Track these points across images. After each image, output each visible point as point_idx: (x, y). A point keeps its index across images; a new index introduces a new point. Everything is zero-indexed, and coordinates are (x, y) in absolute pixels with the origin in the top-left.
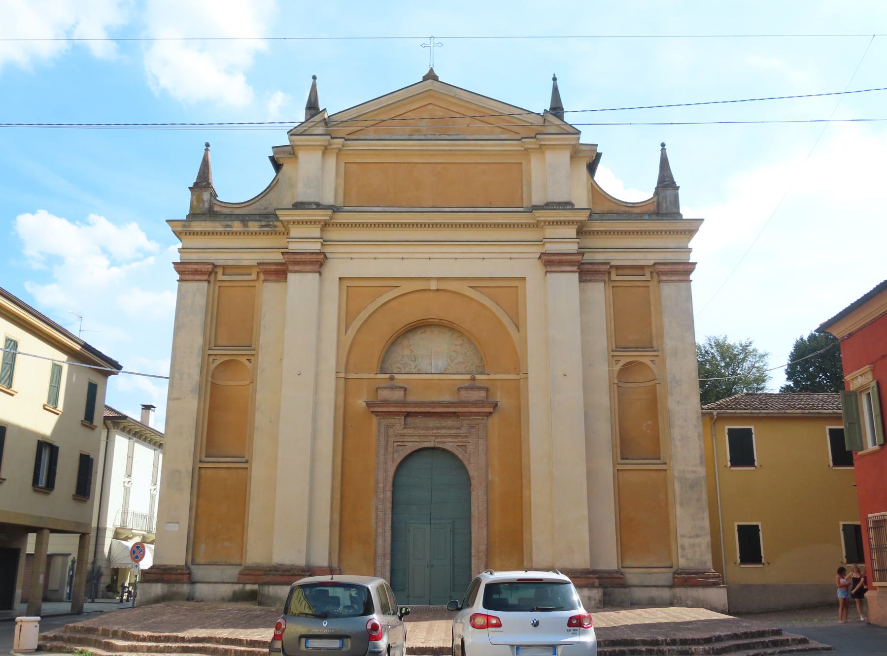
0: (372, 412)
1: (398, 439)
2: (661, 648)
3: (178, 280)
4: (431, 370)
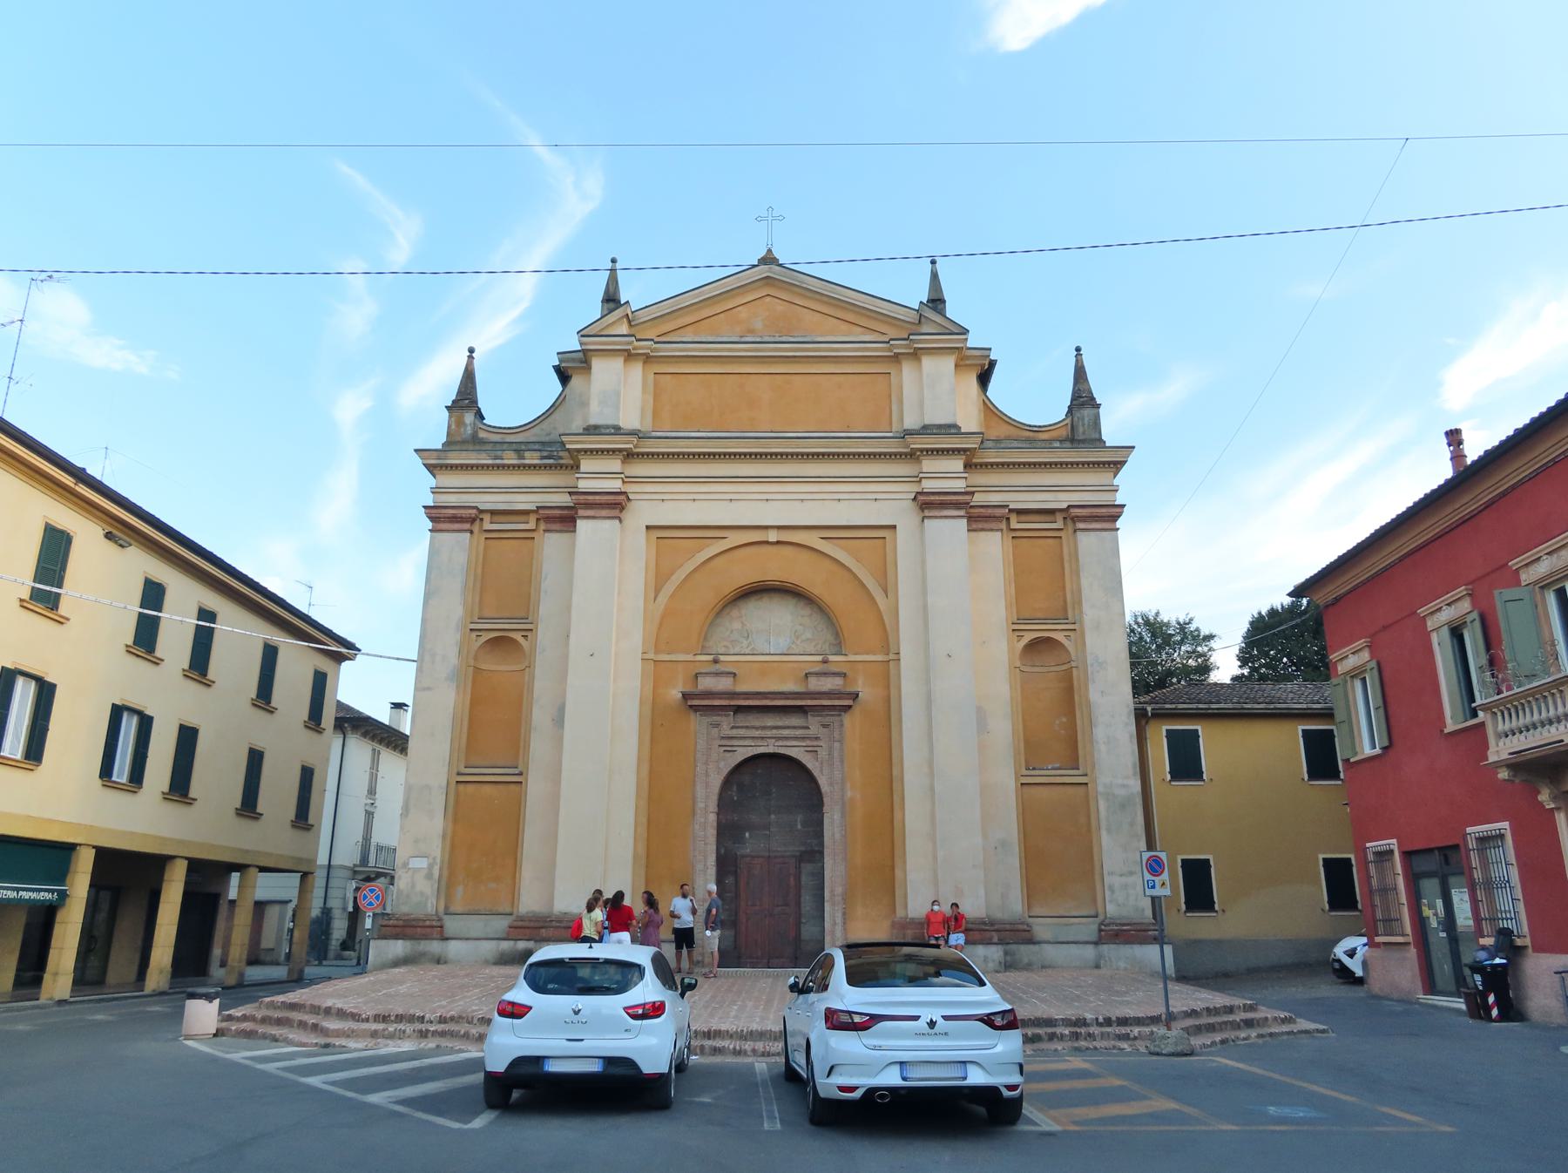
0: (691, 706)
2: (1091, 1030)
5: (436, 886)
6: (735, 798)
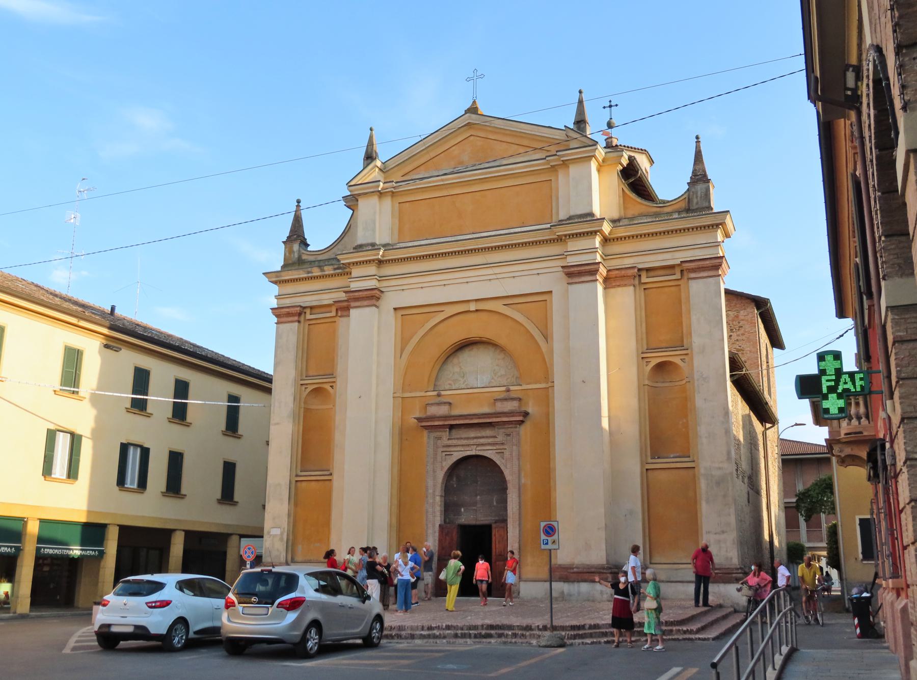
1: (445, 449)
3: (275, 323)
4: (477, 384)
5: (285, 545)
6: (455, 486)
